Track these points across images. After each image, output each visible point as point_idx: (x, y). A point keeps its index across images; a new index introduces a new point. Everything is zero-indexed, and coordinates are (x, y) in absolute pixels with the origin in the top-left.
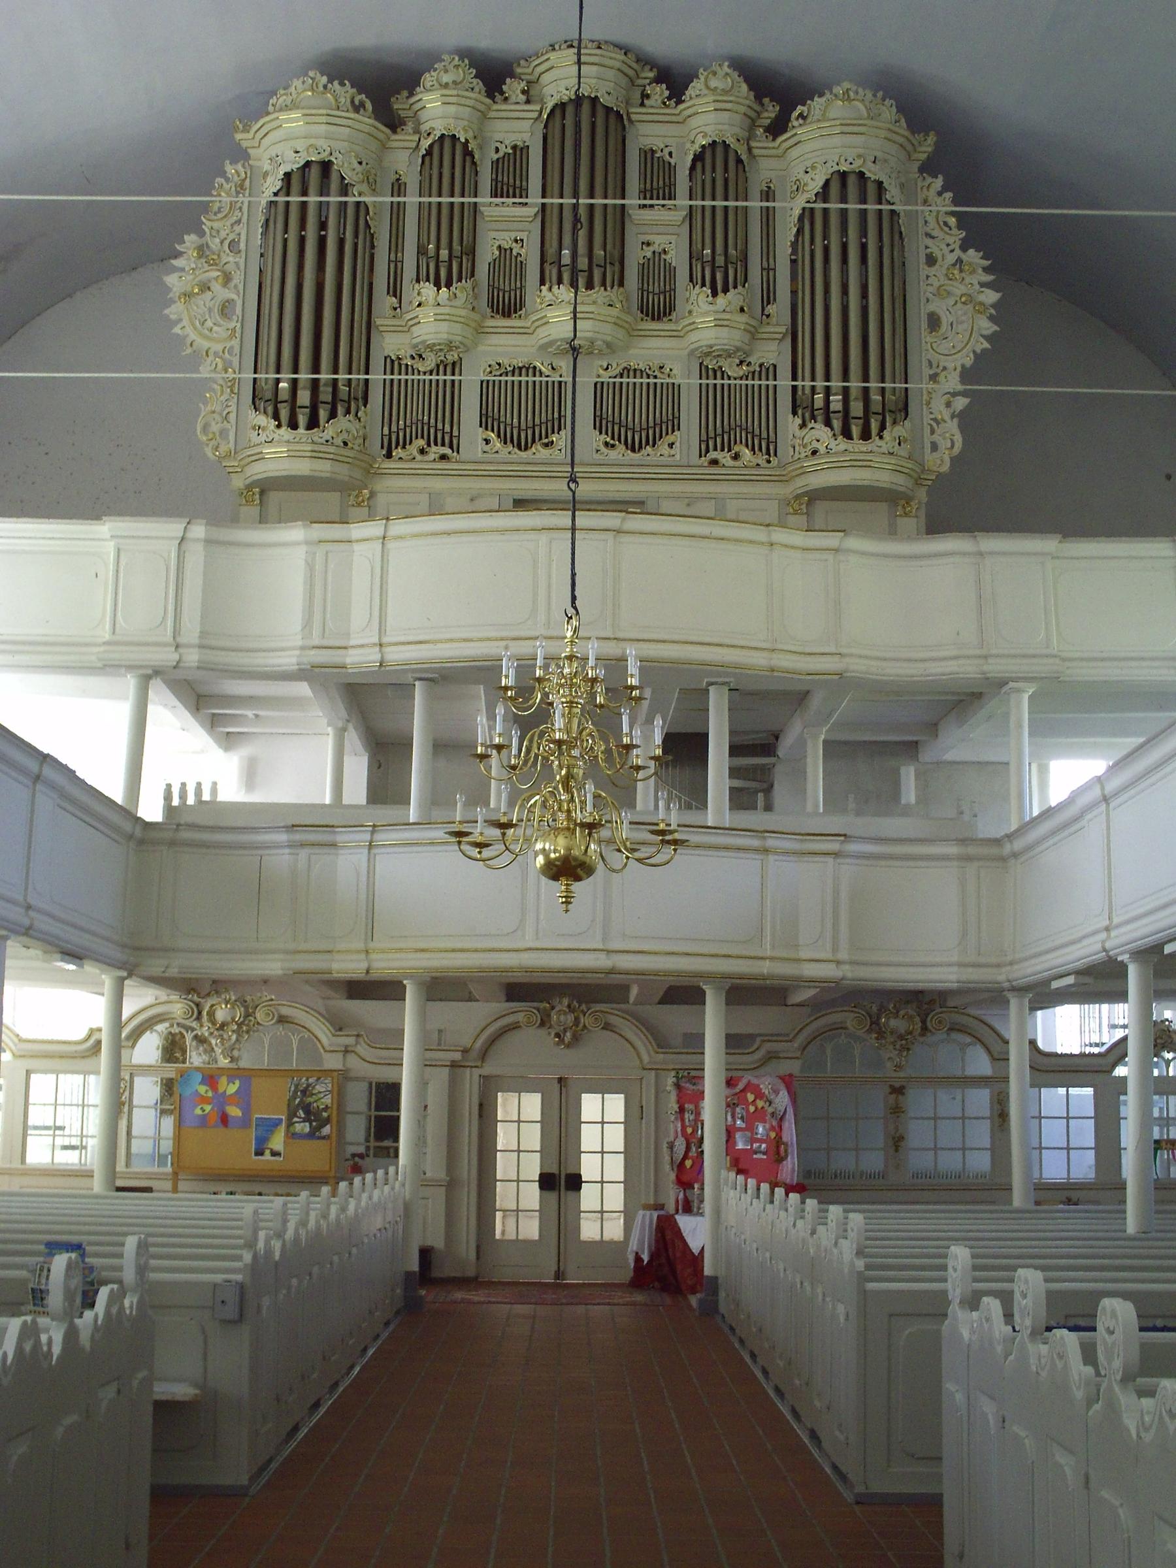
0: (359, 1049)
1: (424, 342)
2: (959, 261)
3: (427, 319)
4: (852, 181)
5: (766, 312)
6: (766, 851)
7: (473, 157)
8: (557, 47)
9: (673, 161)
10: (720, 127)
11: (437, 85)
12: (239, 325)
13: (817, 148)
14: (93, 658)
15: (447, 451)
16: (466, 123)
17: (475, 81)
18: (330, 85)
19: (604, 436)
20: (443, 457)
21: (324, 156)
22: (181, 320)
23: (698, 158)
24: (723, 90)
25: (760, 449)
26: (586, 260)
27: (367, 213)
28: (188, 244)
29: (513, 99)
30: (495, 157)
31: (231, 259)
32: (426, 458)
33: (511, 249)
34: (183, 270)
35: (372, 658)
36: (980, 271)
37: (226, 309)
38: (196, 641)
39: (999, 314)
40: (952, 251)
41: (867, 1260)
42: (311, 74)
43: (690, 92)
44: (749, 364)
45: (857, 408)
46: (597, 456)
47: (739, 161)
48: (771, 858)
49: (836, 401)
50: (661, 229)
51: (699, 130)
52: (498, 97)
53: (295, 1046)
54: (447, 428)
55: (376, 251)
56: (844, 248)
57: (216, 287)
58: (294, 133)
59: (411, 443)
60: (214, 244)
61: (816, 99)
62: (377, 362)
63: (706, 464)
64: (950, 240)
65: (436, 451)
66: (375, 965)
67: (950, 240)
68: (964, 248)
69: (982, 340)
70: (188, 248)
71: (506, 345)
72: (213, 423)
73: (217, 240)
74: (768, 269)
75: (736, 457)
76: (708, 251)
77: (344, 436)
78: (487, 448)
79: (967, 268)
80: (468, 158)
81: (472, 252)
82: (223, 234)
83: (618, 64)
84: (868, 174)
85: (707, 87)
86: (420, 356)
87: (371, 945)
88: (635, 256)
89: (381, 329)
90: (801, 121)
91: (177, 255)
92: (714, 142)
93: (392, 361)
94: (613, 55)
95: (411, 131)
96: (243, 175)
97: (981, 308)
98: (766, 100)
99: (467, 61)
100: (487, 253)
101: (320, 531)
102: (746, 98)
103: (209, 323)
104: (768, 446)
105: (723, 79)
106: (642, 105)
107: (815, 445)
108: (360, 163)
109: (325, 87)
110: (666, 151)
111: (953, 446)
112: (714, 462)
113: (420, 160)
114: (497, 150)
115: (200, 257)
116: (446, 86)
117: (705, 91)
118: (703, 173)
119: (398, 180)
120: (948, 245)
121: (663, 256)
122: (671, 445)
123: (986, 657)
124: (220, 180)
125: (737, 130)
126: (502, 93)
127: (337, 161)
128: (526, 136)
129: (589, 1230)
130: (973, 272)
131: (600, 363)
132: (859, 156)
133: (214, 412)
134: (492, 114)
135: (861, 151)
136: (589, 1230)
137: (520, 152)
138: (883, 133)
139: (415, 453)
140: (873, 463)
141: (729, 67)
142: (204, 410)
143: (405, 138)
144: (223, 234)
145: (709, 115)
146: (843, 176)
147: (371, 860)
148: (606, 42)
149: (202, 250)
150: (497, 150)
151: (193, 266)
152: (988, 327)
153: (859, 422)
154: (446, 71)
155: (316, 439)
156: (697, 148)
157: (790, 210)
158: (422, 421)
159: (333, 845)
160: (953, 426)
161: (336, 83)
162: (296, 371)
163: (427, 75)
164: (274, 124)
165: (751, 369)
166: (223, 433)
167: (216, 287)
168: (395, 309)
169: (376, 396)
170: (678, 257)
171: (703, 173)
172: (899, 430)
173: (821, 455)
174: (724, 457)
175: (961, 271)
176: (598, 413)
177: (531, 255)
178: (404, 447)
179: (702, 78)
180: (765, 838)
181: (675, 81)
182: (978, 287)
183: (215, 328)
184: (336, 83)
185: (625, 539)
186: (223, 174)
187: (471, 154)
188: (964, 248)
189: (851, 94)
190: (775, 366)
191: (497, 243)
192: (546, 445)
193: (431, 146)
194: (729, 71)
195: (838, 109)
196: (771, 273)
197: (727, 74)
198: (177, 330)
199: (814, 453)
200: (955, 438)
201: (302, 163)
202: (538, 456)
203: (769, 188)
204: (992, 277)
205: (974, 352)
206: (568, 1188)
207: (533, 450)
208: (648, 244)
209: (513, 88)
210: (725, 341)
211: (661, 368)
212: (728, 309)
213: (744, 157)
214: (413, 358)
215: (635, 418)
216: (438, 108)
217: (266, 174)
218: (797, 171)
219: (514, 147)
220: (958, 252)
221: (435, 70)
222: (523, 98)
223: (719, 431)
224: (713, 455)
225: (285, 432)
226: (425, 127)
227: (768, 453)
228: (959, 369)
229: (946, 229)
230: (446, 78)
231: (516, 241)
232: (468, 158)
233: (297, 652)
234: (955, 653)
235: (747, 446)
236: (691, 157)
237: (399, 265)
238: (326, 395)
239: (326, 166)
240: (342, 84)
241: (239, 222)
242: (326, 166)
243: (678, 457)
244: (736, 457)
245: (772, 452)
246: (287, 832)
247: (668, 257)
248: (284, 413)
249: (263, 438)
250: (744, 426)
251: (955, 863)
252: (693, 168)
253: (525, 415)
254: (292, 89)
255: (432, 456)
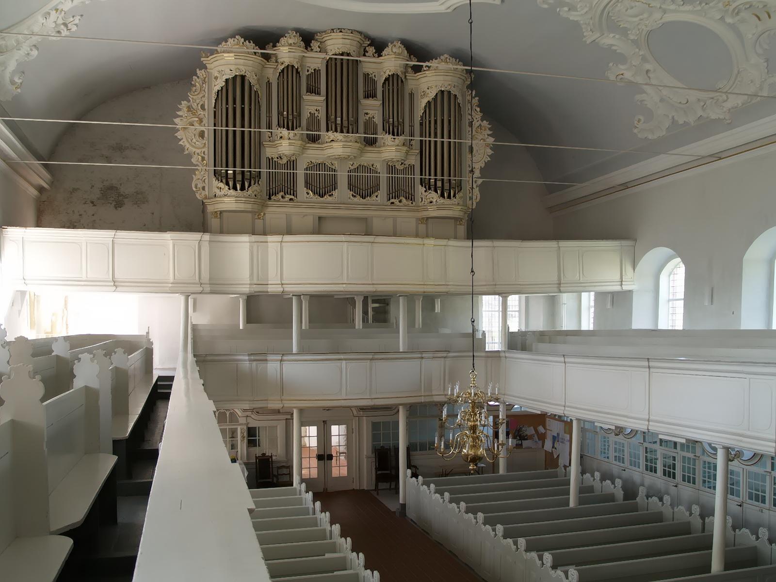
0: (252, 416)
1: (283, 154)
2: (480, 125)
3: (284, 144)
4: (446, 94)
5: (411, 144)
6: (422, 358)
7: (300, 74)
8: (335, 31)
9: (376, 79)
10: (396, 68)
11: (287, 44)
12: (207, 142)
13: (432, 81)
14: (168, 289)
15: (292, 197)
16: (297, 60)
17: (302, 42)
18: (245, 43)
19: (352, 192)
20: (291, 199)
21: (243, 73)
22: (182, 139)
23: (387, 79)
24: (398, 53)
25: (409, 199)
26: (347, 122)
27: (259, 97)
28: (183, 105)
29: (315, 50)
30: (307, 73)
31: (201, 113)
32: (284, 200)
33: (314, 114)
34: (182, 116)
35: (279, 290)
36: (487, 129)
37: (202, 135)
38: (208, 282)
39: (494, 148)
40: (478, 121)
41: (513, 539)
42: (237, 37)
43: (384, 53)
44: (405, 164)
45: (447, 186)
46: (349, 200)
47: (402, 81)
48: (424, 360)
49: (439, 184)
50: (372, 109)
51: (387, 68)
52: (309, 49)
53: (228, 416)
54: (292, 188)
55: (261, 112)
56: (443, 121)
57: (196, 124)
58: (229, 62)
59: (278, 194)
60: (194, 106)
61: (434, 60)
62: (264, 162)
63: (390, 204)
64: (477, 117)
65: (288, 197)
66: (285, 405)
67: (477, 117)
68: (482, 120)
69: (487, 157)
70: (183, 107)
71: (315, 154)
72: (199, 184)
73: (196, 104)
74: (412, 126)
75: (400, 201)
76: (391, 120)
77: (255, 193)
78: (308, 196)
79: (483, 128)
80: (298, 75)
81: (299, 115)
82: (198, 101)
83: (358, 40)
84: (452, 92)
85: (392, 51)
86: (281, 157)
87: (283, 397)
88: (362, 119)
89: (265, 146)
90: (427, 68)
91: (180, 110)
92: (394, 74)
93: (269, 159)
94: (357, 36)
95: (274, 61)
96: (205, 76)
97: (487, 145)
98: (412, 56)
99: (298, 34)
100: (305, 115)
101: (254, 238)
102: (407, 57)
103: (194, 140)
104: (411, 197)
105: (398, 48)
106: (364, 55)
107: (431, 200)
108: (256, 76)
109: (243, 43)
110: (373, 75)
111: (476, 199)
112: (392, 203)
113: (278, 74)
114: (308, 71)
115: (188, 111)
116: (290, 45)
117: (391, 53)
118: (389, 86)
119: (269, 81)
120: (476, 119)
121: (372, 119)
122: (377, 196)
123: (495, 285)
124: (195, 77)
125: (402, 69)
126: (310, 47)
127: (248, 75)
128: (319, 65)
129: (335, 472)
130: (485, 130)
131: (350, 162)
132: (449, 85)
133: (199, 179)
134: (409, 154)
135: (450, 83)
136: (335, 472)
137: (317, 72)
138: (459, 76)
139: (280, 197)
140: (453, 208)
141: (400, 44)
142: (195, 178)
143: (271, 65)
144: (198, 101)
145: (391, 62)
146: (442, 92)
147: (281, 366)
148: (355, 30)
149: (189, 108)
150: (308, 71)
151: (186, 115)
152: (490, 152)
153: (447, 190)
154: (290, 38)
155: (245, 194)
156: (386, 75)
157: (421, 104)
158: (281, 185)
159: (266, 360)
160: (476, 191)
161: (247, 41)
162: (235, 167)
163: (282, 38)
164: (221, 57)
165: (406, 166)
166: (204, 188)
167: (196, 124)
168: (270, 137)
169: (264, 177)
170: (378, 120)
171: (389, 86)
172: (461, 194)
173: (432, 204)
174: (396, 201)
175: (481, 129)
176: (349, 183)
177: (322, 116)
178: (276, 195)
179: (390, 47)
180: (422, 354)
181: (379, 46)
182: (486, 136)
183: (197, 143)
184: (247, 41)
185: (375, 245)
186: (196, 75)
187: (299, 73)
188: (482, 120)
189: (448, 61)
190: (414, 166)
191: (310, 111)
192: (330, 195)
193: (283, 69)
194: (401, 45)
195: (443, 66)
196: (413, 127)
197: (400, 47)
198: (181, 143)
199: (431, 202)
200: (478, 196)
201: (234, 75)
202: (327, 200)
203: (412, 92)
204: (491, 132)
205: (485, 161)
206: (327, 460)
207: (325, 197)
208: (367, 114)
209: (315, 45)
210: (399, 157)
211: (373, 165)
212: (399, 145)
213: (404, 80)
214: (277, 158)
215: (363, 186)
216: (287, 53)
217: (216, 78)
218: (424, 87)
219: (315, 70)
220: (480, 121)
221: (286, 37)
222: (318, 50)
223: (394, 191)
224: (392, 201)
225: (232, 192)
226: (280, 60)
227: (411, 200)
228: (480, 168)
229: (476, 112)
230: (291, 41)
231: (316, 110)
232: (298, 75)
233: (248, 286)
234: (484, 283)
235: (404, 197)
236: (384, 79)
237: (270, 118)
238: (247, 175)
239: (243, 77)
240: (250, 42)
241: (204, 96)
242: (243, 77)
243: (379, 201)
244: (400, 201)
245: (413, 200)
246: (248, 356)
247: (374, 120)
248: (231, 183)
249: (222, 193)
250: (407, 192)
251: (484, 358)
252: (384, 83)
253: (322, 183)
254: (228, 43)
255: (287, 199)
